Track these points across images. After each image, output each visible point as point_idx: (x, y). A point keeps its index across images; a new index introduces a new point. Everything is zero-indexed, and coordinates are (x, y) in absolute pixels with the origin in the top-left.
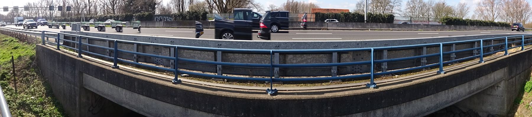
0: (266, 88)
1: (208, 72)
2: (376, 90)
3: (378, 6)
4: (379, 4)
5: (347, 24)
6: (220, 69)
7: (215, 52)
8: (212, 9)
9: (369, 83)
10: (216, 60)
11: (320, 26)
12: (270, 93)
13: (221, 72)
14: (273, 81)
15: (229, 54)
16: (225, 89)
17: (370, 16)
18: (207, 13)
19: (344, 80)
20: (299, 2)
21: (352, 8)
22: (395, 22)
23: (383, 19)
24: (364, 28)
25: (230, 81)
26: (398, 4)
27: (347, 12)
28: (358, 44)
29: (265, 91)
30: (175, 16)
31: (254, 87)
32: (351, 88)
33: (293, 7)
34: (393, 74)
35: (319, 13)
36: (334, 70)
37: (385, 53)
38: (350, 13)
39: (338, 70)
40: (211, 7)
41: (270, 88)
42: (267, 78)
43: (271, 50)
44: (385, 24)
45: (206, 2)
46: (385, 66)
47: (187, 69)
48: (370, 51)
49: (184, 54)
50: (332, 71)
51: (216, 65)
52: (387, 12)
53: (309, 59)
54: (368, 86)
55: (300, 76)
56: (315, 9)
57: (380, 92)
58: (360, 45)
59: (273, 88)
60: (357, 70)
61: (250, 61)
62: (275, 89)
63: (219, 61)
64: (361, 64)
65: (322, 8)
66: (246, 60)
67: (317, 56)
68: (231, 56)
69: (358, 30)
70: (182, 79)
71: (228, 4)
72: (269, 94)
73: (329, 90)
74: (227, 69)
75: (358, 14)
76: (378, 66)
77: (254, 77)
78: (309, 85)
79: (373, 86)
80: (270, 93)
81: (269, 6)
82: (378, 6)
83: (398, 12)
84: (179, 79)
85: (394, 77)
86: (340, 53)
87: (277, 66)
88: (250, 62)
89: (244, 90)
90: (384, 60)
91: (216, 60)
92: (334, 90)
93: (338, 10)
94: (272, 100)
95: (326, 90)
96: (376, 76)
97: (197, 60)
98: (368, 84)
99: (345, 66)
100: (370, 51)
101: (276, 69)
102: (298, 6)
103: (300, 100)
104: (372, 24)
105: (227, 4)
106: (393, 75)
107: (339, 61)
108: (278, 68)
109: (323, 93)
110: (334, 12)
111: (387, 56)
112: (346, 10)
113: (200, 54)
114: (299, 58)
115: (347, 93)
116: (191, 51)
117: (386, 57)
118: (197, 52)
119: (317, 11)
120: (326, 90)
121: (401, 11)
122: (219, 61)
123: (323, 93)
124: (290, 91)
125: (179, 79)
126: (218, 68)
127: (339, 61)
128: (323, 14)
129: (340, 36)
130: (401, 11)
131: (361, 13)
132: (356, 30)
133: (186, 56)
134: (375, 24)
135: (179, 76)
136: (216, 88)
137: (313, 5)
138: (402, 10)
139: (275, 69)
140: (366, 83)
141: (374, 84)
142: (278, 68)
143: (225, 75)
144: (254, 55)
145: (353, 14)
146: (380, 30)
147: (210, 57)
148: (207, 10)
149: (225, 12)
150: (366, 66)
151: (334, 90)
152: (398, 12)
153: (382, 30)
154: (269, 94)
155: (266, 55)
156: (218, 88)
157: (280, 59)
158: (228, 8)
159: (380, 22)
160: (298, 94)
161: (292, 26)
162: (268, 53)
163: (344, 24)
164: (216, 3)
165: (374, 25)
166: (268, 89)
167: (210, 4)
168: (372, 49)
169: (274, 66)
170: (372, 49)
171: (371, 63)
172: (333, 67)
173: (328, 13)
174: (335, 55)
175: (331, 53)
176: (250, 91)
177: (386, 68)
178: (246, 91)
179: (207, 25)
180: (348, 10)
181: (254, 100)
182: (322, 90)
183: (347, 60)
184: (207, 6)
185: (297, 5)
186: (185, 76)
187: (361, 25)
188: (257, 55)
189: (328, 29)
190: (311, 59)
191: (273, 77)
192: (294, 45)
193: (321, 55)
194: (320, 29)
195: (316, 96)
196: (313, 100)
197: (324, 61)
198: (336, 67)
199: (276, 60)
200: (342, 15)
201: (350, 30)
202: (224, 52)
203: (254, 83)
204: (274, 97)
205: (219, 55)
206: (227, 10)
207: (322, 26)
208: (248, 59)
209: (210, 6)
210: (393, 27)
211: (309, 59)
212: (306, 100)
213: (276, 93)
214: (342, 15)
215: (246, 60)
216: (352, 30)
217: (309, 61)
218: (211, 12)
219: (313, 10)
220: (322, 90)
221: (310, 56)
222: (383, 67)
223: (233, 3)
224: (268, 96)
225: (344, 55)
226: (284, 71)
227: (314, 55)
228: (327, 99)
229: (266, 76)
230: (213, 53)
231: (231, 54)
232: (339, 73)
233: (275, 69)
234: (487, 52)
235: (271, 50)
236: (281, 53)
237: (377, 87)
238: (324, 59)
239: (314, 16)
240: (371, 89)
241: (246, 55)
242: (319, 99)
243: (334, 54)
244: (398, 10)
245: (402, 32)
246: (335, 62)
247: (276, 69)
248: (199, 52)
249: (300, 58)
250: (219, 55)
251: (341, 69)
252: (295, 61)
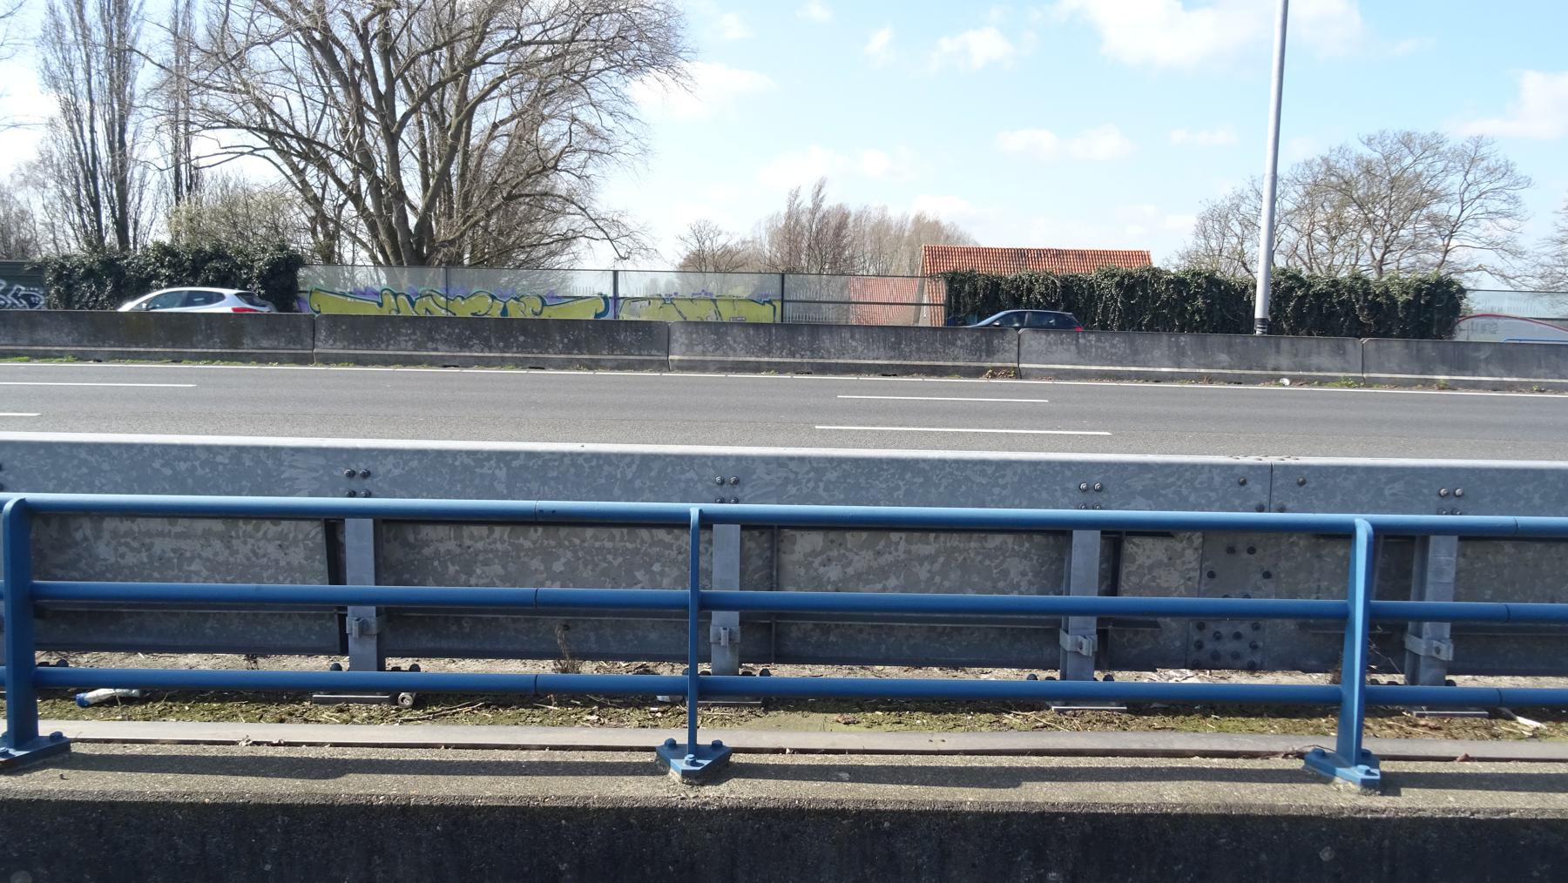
0: (657, 738)
1: (291, 651)
2: (1380, 802)
3: (1342, 227)
4: (1351, 212)
5: (1143, 341)
6: (363, 628)
7: (332, 522)
8: (332, 237)
9: (1330, 744)
10: (336, 572)
11: (974, 351)
12: (680, 765)
13: (371, 648)
14: (705, 693)
15: (428, 532)
16: (394, 755)
17: (1286, 288)
18: (292, 262)
19: (1140, 705)
20: (853, 207)
21: (1169, 248)
22: (1465, 332)
23: (1374, 307)
24: (1250, 369)
25: (435, 698)
26: (1494, 204)
27: (1135, 267)
28: (1240, 479)
29: (649, 758)
30: (64, 273)
31: (586, 733)
32: (1197, 762)
33: (818, 239)
34: (1499, 708)
35: (971, 277)
36: (1078, 638)
37: (1443, 555)
38: (1156, 273)
39: (1102, 634)
40: (328, 227)
41: (682, 738)
42: (664, 670)
43: (694, 510)
44: (1396, 346)
45: (291, 192)
46: (1432, 642)
47: (132, 649)
48: (1346, 534)
49: (103, 550)
50: (1067, 641)
51: (338, 608)
52: (1407, 266)
53: (921, 560)
54: (1319, 768)
55: (865, 662)
56: (946, 253)
57: (1417, 825)
58: (1255, 487)
59: (705, 738)
60: (1229, 646)
61: (558, 567)
62: (717, 745)
63: (361, 578)
64: (1256, 617)
65: (985, 244)
66: (536, 564)
67: (974, 543)
68: (441, 539)
69: (1211, 379)
70: (71, 729)
71: (439, 207)
72: (674, 775)
73: (1055, 762)
74: (408, 625)
75: (1212, 280)
76: (1388, 639)
77: (588, 668)
78: (920, 719)
79: (1359, 772)
80: (680, 765)
81: (686, 232)
82: (1342, 227)
83: (1489, 258)
84: (45, 728)
85: (1502, 727)
86: (1116, 536)
87: (724, 604)
88: (564, 579)
89: (523, 756)
90: (1429, 602)
91: (336, 572)
92: (1083, 762)
93: (1081, 255)
94: (696, 815)
95: (1036, 761)
96: (1379, 705)
97: (201, 583)
98: (1322, 754)
99: (1147, 619)
100: (1346, 534)
101: (723, 623)
102: (849, 232)
103: (867, 820)
104: (1305, 343)
105: (429, 206)
106: (1495, 714)
107: (1112, 584)
108: (734, 617)
109: (1013, 777)
110: (1048, 266)
111: (1449, 577)
112: (1128, 255)
113: (226, 539)
114: (860, 553)
115: (1173, 795)
116: (156, 524)
117: (1440, 582)
118: (201, 525)
119: (955, 264)
120: (1036, 761)
121: (1517, 254)
122: (361, 578)
123: (1013, 777)
124: (808, 752)
125: (45, 728)
126: (352, 626)
127: (1112, 584)
128: (995, 285)
129: (1099, 419)
130: (1517, 254)
131: (1228, 271)
132: (1199, 378)
133: (114, 567)
134: (1327, 344)
135: (42, 707)
136: (337, 754)
137: (935, 227)
138: (1524, 242)
139: (717, 616)
140: (1307, 743)
141: (1366, 758)
142: (734, 617)
143: (405, 663)
144: (589, 532)
145: (1179, 282)
146: (1358, 382)
147: (297, 556)
148: (303, 243)
149: (420, 260)
150: (1290, 625)
151: (1083, 762)
152: (1489, 258)
153: (1369, 383)
154: (674, 775)
155: (661, 534)
156: (350, 754)
157: (744, 558)
158: (440, 230)
159: (1358, 331)
160: (859, 774)
161: (814, 352)
162: (677, 522)
163: (1118, 343)
164: (356, 198)
165: (1320, 351)
166: (672, 745)
167: (317, 202)
168: (1363, 525)
169: (708, 604)
170: (1363, 525)
171: (1345, 617)
172: (1074, 621)
173: (1024, 274)
174: (1086, 552)
175: (1061, 532)
176: (558, 757)
177: (1447, 653)
178: (535, 756)
179: (296, 340)
180: (1144, 256)
181: (578, 817)
182: (1006, 761)
183: (1162, 582)
184: (300, 216)
185: (842, 225)
186: (110, 702)
187: (1229, 349)
188: (604, 533)
189: (1019, 374)
190: (932, 559)
191: (704, 667)
192: (832, 476)
193: (996, 540)
194: (978, 372)
195: (969, 798)
196: (950, 821)
197: (1013, 582)
198: (1094, 620)
199: (725, 568)
200: (1109, 288)
201: (1159, 378)
202: (386, 521)
203: (587, 704)
204: (710, 792)
205: (359, 542)
206: (433, 250)
207: (991, 352)
208: (549, 556)
209: (320, 218)
210: (1463, 359)
211: (921, 560)
212: (906, 820)
213: (718, 764)
214: (1109, 288)
215: (536, 564)
216: (1171, 378)
217: (923, 572)
218: (329, 255)
219: (935, 254)
220: (1006, 761)
221: (929, 545)
222: (1417, 646)
223: (466, 203)
224: (669, 788)
225: (1148, 542)
226: (771, 631)
227: (955, 540)
228: (1044, 823)
229: (661, 659)
230: (315, 531)
231: (441, 531)
232: (1108, 657)
233: (717, 616)
234: (1346, 379)
235: (694, 510)
236: (749, 524)
237: (1389, 785)
238: (1015, 567)
239: (941, 292)
240: (1345, 793)
241: (537, 533)
242: (987, 820)
243: (1077, 535)
244: (1493, 245)
245: (1528, 399)
246: (1083, 587)
247: (723, 623)
248: (217, 526)
249: (868, 555)
250: (359, 542)
251: (1124, 637)
252: (833, 573)
